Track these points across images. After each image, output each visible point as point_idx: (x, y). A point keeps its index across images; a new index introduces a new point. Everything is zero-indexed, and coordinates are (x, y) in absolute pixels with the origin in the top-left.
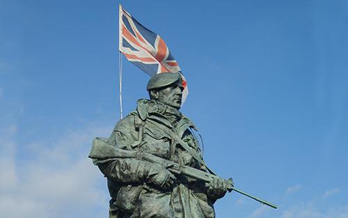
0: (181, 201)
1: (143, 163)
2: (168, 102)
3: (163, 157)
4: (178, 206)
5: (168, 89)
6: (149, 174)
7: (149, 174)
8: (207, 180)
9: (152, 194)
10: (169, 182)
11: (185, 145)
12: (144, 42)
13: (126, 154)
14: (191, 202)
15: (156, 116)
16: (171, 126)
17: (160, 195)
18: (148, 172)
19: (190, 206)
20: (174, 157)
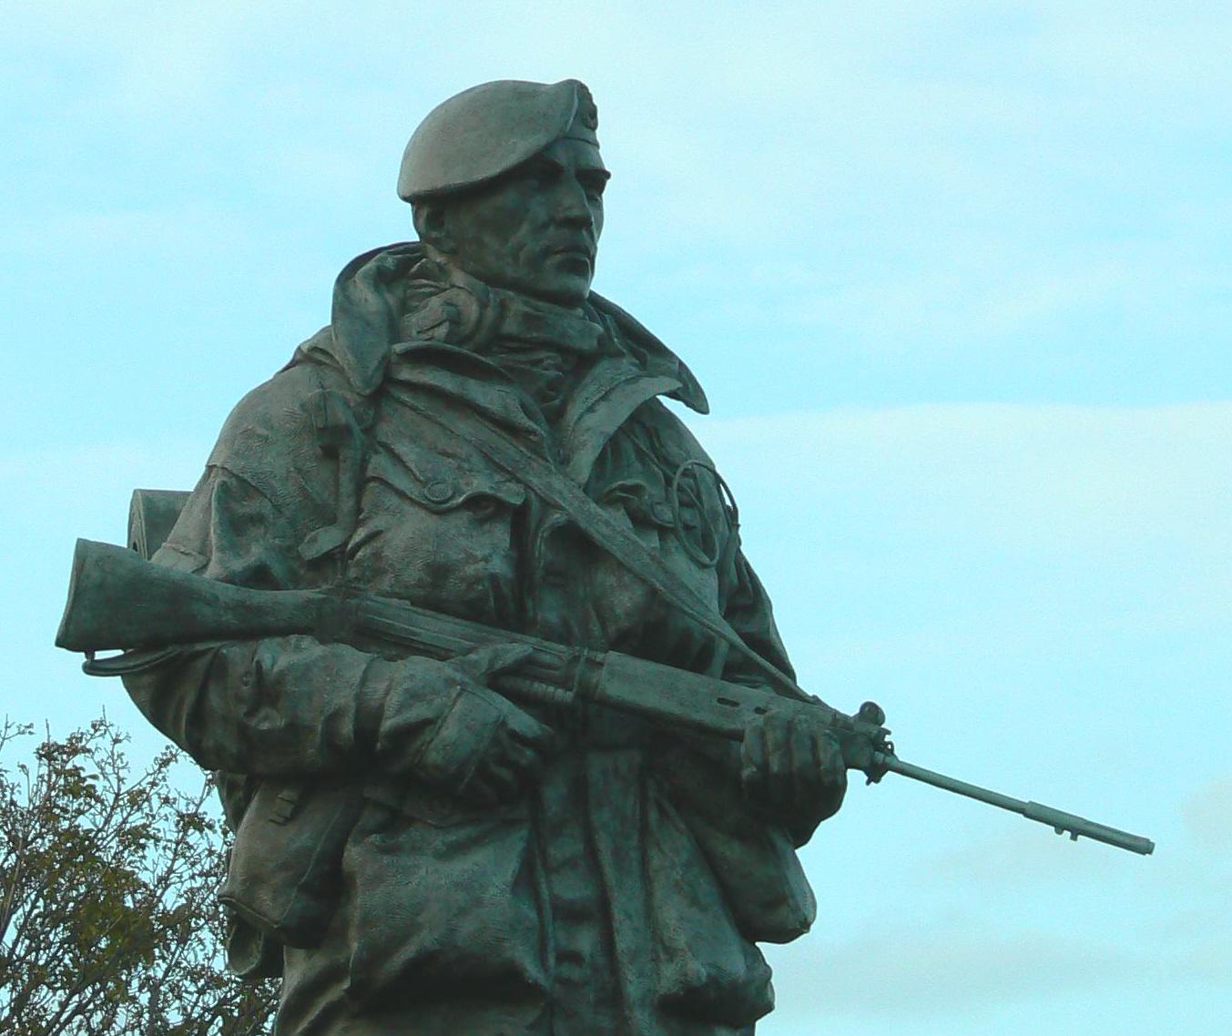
0: (592, 852)
1: (354, 661)
2: (510, 272)
3: (472, 611)
4: (572, 888)
5: (509, 198)
6: (387, 725)
7: (387, 725)
8: (728, 725)
9: (416, 833)
10: (503, 761)
11: (609, 525)
12: (426, 340)
13: (259, 610)
14: (653, 852)
15: (511, 926)
16: (522, 419)
17: (452, 838)
18: (379, 714)
19: (104, 711)
20: (550, 610)
